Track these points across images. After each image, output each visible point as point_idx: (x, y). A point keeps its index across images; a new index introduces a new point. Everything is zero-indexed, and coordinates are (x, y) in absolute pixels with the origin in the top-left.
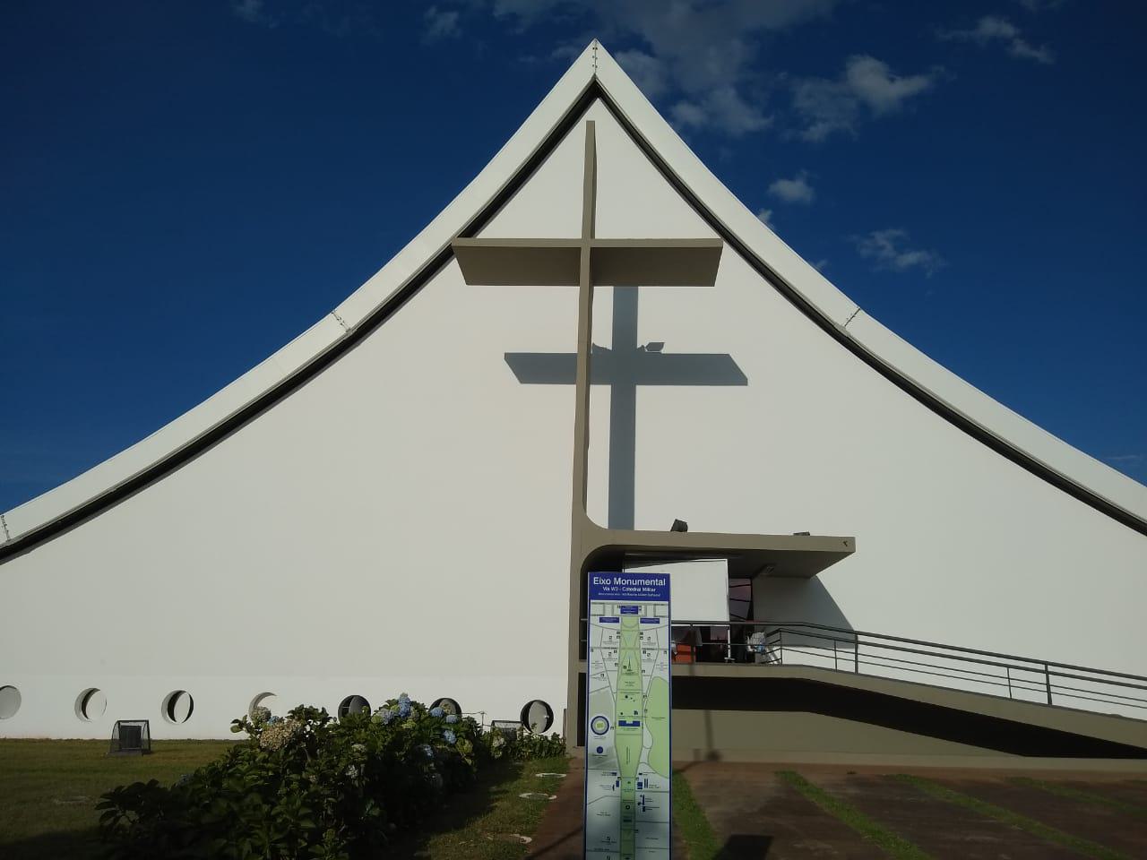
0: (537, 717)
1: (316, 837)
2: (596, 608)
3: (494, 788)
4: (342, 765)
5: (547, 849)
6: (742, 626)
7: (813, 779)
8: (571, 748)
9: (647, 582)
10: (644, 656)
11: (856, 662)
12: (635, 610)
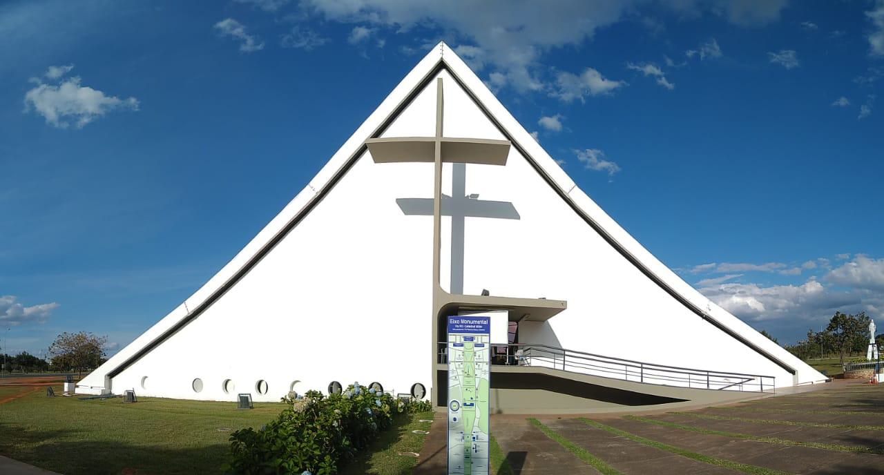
0: (418, 391)
1: (321, 459)
2: (452, 338)
3: (400, 428)
4: (330, 422)
5: (426, 461)
6: (512, 349)
7: (544, 422)
8: (436, 408)
9: (478, 322)
10: (477, 366)
11: (564, 364)
12: (472, 339)
